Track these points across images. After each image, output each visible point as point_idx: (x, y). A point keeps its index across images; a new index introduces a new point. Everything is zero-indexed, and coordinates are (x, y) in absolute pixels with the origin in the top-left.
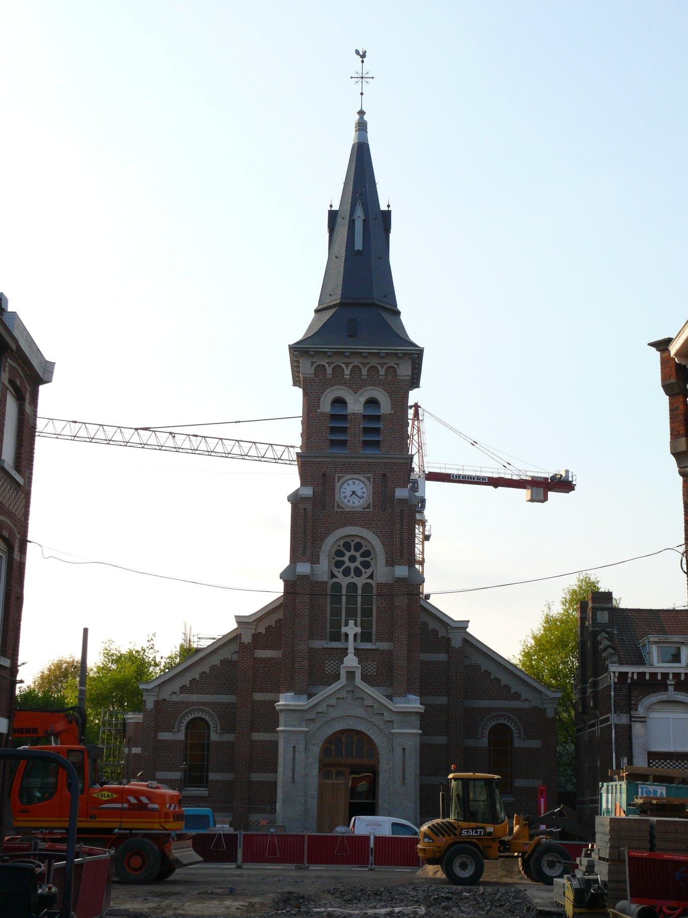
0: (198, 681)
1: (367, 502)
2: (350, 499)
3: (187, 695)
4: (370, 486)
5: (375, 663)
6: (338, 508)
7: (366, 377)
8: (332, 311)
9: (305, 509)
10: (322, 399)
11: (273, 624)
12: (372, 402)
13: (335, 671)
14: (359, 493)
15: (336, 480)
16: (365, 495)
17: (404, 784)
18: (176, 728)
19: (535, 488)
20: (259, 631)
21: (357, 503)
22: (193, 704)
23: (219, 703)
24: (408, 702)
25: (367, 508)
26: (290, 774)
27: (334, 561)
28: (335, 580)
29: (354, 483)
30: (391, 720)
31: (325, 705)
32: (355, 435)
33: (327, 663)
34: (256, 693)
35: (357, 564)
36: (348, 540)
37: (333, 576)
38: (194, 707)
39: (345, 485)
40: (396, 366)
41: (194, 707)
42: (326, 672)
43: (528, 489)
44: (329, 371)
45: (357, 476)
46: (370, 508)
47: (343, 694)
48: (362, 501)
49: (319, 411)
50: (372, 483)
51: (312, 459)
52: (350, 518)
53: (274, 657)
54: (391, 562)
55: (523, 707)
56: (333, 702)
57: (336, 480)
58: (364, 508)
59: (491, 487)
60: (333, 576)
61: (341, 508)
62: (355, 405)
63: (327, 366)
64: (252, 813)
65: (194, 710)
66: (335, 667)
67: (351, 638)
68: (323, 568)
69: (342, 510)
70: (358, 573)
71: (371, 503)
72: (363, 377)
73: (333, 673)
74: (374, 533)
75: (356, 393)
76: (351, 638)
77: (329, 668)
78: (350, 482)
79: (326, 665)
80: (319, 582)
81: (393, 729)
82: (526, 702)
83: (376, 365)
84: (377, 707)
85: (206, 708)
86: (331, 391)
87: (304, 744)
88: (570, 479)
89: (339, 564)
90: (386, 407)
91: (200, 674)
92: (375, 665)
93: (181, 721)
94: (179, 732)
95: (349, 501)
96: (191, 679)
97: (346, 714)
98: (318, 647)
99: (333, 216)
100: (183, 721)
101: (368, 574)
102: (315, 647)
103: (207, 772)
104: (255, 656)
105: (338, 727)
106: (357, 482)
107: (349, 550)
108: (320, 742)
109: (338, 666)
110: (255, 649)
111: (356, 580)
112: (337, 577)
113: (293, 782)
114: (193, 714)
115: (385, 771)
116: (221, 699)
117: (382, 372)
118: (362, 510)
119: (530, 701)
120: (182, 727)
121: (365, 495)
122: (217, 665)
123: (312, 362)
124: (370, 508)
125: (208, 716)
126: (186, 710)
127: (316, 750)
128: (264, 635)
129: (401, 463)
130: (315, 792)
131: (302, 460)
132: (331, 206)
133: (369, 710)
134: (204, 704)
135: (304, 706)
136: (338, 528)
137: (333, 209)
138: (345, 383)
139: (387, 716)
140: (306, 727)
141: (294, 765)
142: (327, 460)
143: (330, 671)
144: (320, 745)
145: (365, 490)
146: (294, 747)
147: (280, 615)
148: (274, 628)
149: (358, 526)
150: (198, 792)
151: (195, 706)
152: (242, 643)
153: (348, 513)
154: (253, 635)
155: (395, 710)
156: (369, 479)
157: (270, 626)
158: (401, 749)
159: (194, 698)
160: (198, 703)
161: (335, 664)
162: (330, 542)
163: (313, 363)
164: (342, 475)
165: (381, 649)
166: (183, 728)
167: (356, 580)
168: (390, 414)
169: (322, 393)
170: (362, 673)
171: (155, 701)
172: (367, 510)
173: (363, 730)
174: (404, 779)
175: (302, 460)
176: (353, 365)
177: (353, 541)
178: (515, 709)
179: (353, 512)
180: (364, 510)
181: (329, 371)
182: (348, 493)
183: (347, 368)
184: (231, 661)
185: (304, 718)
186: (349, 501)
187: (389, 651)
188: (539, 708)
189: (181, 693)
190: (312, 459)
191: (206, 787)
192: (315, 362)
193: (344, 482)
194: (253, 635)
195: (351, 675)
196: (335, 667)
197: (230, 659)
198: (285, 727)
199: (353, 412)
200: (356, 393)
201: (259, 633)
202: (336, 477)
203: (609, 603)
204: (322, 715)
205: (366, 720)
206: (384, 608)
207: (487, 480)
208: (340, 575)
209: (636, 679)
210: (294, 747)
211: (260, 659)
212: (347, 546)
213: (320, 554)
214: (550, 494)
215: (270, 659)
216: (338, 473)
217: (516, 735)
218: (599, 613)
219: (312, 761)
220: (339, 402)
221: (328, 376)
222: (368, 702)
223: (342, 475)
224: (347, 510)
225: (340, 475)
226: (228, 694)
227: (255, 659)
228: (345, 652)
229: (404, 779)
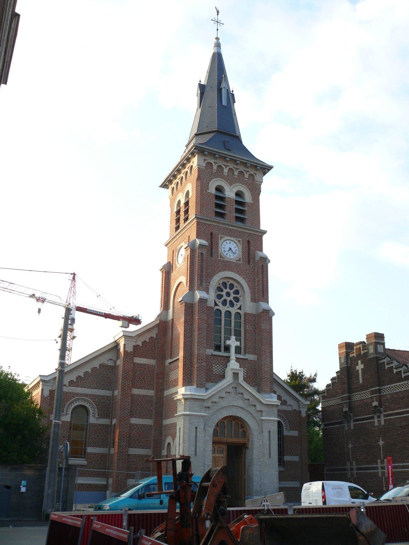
0: (82, 378)
1: (238, 257)
2: (228, 253)
3: (74, 387)
4: (241, 247)
6: (220, 257)
7: (236, 177)
8: (211, 135)
9: (202, 254)
10: (210, 184)
11: (148, 340)
12: (239, 194)
13: (219, 372)
14: (233, 249)
15: (219, 239)
16: (237, 252)
17: (270, 457)
18: (64, 412)
19: (124, 321)
20: (138, 344)
21: (232, 257)
22: (78, 394)
23: (97, 396)
24: (271, 398)
25: (239, 261)
26: (194, 449)
27: (217, 294)
28: (217, 307)
29: (230, 243)
30: (261, 410)
31: (217, 396)
32: (230, 211)
33: (214, 366)
34: (135, 389)
35: (228, 299)
36: (226, 281)
37: (216, 304)
38: (78, 397)
39: (224, 243)
40: (254, 175)
41: (78, 397)
42: (214, 373)
43: (121, 321)
44: (215, 167)
45: (232, 239)
46: (240, 261)
47: (230, 390)
48: (235, 255)
49: (208, 191)
50: (241, 244)
51: (205, 222)
52: (227, 265)
53: (147, 363)
54: (254, 300)
55: (288, 410)
56: (223, 394)
57: (219, 239)
58: (237, 261)
59: (104, 318)
60: (216, 304)
61: (222, 258)
62: (230, 193)
63: (213, 164)
64: (129, 478)
65: (78, 400)
66: (219, 370)
67: (233, 350)
68: (211, 297)
69: (223, 259)
70: (232, 305)
71: (241, 258)
72: (235, 176)
73: (218, 374)
74: (243, 278)
75: (231, 185)
76: (233, 350)
77: (216, 369)
78: (228, 242)
79: (214, 368)
80: (209, 307)
81: (262, 416)
82: (290, 406)
83: (243, 171)
84: (252, 400)
85: (87, 399)
86: (214, 181)
88: (140, 319)
89: (219, 297)
90: (248, 198)
91: (84, 373)
93: (68, 407)
94: (66, 415)
95: (227, 254)
96: (77, 376)
99: (202, 88)
100: (70, 407)
101: (238, 306)
103: (85, 446)
104: (134, 362)
105: (226, 414)
106: (232, 243)
107: (226, 288)
108: (214, 425)
109: (223, 370)
110: (134, 357)
111: (230, 309)
112: (218, 306)
114: (77, 402)
115: (257, 448)
116: (99, 393)
117: (246, 176)
118: (236, 262)
119: (292, 406)
120: (69, 411)
121: (237, 252)
122: (96, 368)
123: (204, 159)
124: (240, 261)
125: (89, 404)
126: (73, 399)
127: (211, 430)
128: (141, 347)
129: (258, 235)
130: (210, 463)
131: (198, 220)
132: (200, 81)
133: (247, 402)
134: (86, 395)
135: (205, 396)
136: (220, 271)
137: (201, 83)
138: (223, 177)
139: (259, 407)
140: (205, 413)
141: (196, 441)
142: (213, 224)
143: (216, 372)
145: (237, 249)
146: (196, 428)
147: (154, 334)
148: (148, 343)
149: (233, 272)
150: (79, 462)
151: (79, 396)
152: (126, 351)
153: (227, 262)
154: (134, 346)
155: (265, 403)
156: (239, 241)
157: (145, 341)
159: (79, 390)
160: (81, 395)
161: (219, 367)
162: (216, 280)
163: (205, 160)
164: (223, 236)
165: (249, 359)
166: (70, 412)
167: (230, 309)
168: (251, 203)
169: (210, 181)
170: (244, 376)
171: (50, 390)
172: (239, 262)
173: (242, 417)
175: (198, 220)
176: (229, 167)
177: (228, 282)
178: (284, 411)
179: (230, 262)
180: (237, 262)
181: (215, 167)
182: (227, 249)
183: (226, 168)
184: (107, 366)
185: (203, 406)
186: (227, 254)
187: (254, 361)
188: (297, 411)
189: (69, 386)
190: (205, 222)
191: (84, 458)
192: (206, 160)
193: (224, 241)
194: (134, 346)
195: (236, 375)
196: (219, 370)
197: (106, 364)
198: (189, 412)
199: (229, 197)
200: (231, 185)
201: (137, 345)
202: (219, 237)
203: (382, 340)
204: (215, 404)
205: (244, 409)
206: (251, 330)
207: (103, 314)
208: (220, 304)
210: (196, 428)
211: (138, 364)
212: (224, 284)
213: (210, 287)
214: (130, 325)
215: (144, 365)
216: (221, 234)
217: (284, 428)
218: (378, 346)
219: (209, 439)
220: (219, 189)
221: (214, 171)
222: (246, 396)
223: (223, 236)
224: (226, 259)
225: (222, 236)
226: (103, 390)
227: (134, 364)
228: (228, 359)
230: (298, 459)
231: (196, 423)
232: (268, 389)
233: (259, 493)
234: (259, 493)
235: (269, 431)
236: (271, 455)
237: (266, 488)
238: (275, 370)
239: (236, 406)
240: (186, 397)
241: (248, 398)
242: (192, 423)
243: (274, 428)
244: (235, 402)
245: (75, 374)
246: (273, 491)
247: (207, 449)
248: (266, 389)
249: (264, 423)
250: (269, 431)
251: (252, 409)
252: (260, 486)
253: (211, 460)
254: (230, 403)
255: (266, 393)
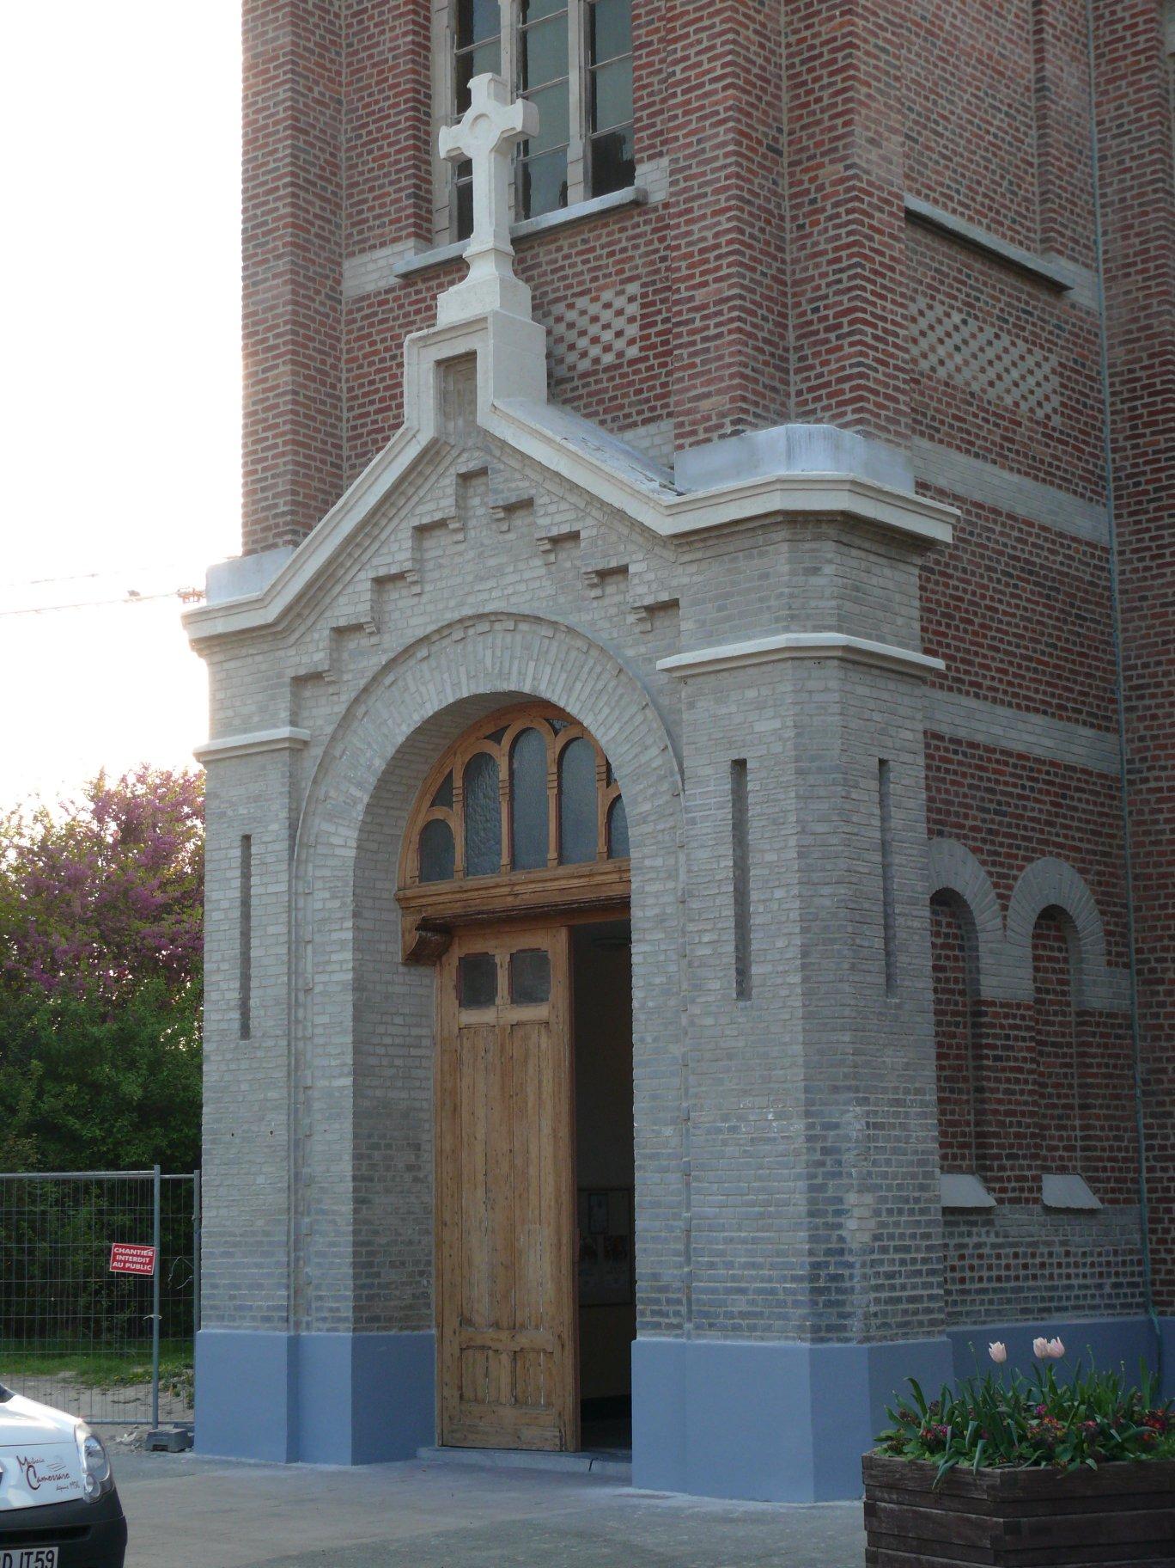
5: (633, 288)
30: (664, 597)
56: (395, 553)
87: (284, 814)
92: (631, 299)
97: (467, 611)
98: (383, 284)
102: (370, 288)
108: (358, 794)
113: (245, 1031)
115: (661, 920)
144: (358, 812)
158: (726, 768)
173: (545, 692)
174: (743, 972)
185: (280, 675)
205: (554, 624)
209: (115, 1266)
210: (247, 839)
219: (329, 905)
229: (743, 972)
230: (1027, 972)
231: (242, 811)
232: (721, 402)
233: (679, 1302)
234: (679, 1302)
235: (740, 766)
236: (755, 970)
237: (712, 1265)
238: (442, 298)
239: (444, 631)
240: (221, 626)
241: (565, 529)
242: (224, 814)
243: (777, 724)
244: (491, 583)
245: (1047, 387)
246: (773, 1292)
247: (324, 978)
248: (705, 405)
249: (691, 706)
250: (740, 766)
251: (613, 611)
252: (681, 1247)
253: (349, 1059)
254: (461, 604)
255: (702, 436)
